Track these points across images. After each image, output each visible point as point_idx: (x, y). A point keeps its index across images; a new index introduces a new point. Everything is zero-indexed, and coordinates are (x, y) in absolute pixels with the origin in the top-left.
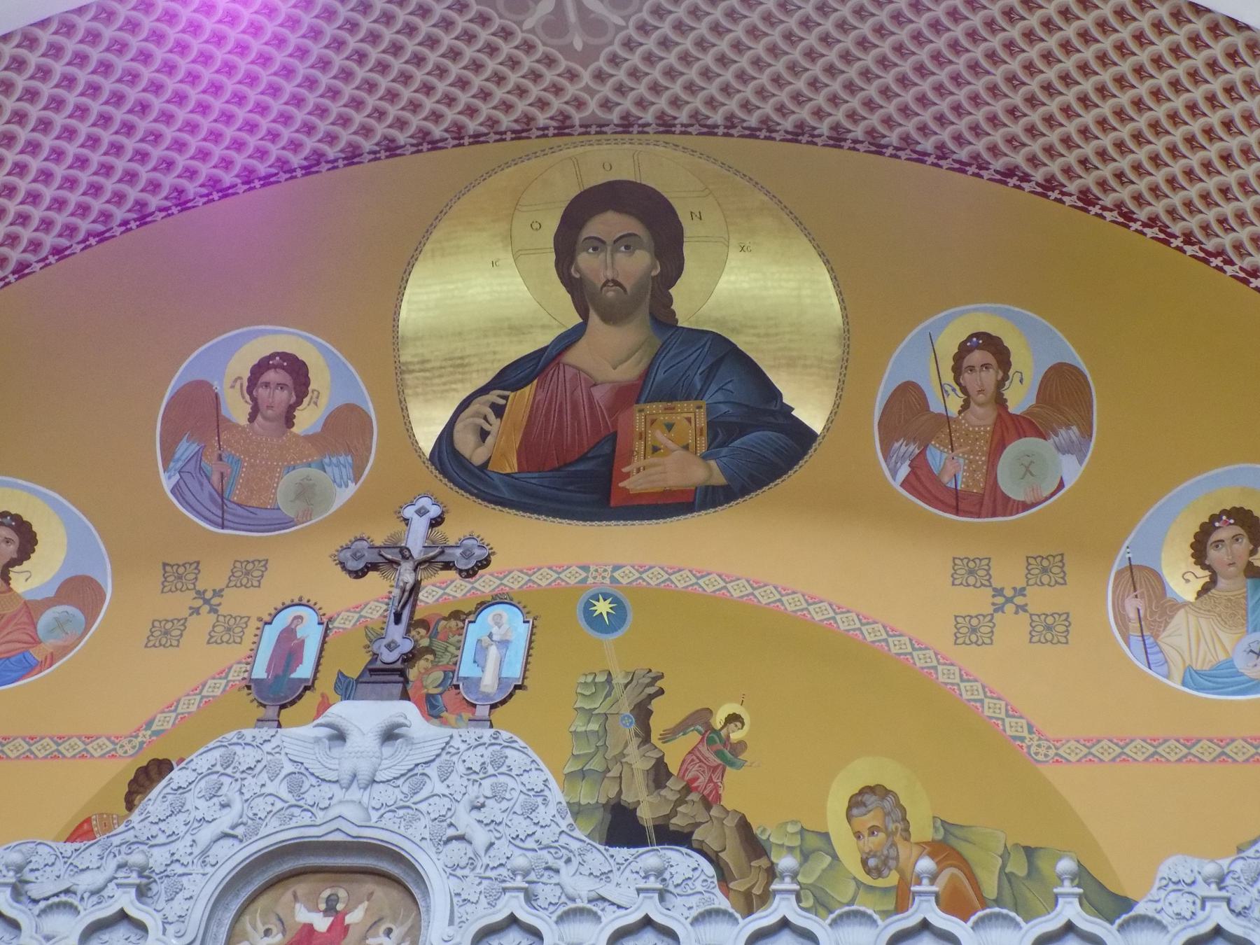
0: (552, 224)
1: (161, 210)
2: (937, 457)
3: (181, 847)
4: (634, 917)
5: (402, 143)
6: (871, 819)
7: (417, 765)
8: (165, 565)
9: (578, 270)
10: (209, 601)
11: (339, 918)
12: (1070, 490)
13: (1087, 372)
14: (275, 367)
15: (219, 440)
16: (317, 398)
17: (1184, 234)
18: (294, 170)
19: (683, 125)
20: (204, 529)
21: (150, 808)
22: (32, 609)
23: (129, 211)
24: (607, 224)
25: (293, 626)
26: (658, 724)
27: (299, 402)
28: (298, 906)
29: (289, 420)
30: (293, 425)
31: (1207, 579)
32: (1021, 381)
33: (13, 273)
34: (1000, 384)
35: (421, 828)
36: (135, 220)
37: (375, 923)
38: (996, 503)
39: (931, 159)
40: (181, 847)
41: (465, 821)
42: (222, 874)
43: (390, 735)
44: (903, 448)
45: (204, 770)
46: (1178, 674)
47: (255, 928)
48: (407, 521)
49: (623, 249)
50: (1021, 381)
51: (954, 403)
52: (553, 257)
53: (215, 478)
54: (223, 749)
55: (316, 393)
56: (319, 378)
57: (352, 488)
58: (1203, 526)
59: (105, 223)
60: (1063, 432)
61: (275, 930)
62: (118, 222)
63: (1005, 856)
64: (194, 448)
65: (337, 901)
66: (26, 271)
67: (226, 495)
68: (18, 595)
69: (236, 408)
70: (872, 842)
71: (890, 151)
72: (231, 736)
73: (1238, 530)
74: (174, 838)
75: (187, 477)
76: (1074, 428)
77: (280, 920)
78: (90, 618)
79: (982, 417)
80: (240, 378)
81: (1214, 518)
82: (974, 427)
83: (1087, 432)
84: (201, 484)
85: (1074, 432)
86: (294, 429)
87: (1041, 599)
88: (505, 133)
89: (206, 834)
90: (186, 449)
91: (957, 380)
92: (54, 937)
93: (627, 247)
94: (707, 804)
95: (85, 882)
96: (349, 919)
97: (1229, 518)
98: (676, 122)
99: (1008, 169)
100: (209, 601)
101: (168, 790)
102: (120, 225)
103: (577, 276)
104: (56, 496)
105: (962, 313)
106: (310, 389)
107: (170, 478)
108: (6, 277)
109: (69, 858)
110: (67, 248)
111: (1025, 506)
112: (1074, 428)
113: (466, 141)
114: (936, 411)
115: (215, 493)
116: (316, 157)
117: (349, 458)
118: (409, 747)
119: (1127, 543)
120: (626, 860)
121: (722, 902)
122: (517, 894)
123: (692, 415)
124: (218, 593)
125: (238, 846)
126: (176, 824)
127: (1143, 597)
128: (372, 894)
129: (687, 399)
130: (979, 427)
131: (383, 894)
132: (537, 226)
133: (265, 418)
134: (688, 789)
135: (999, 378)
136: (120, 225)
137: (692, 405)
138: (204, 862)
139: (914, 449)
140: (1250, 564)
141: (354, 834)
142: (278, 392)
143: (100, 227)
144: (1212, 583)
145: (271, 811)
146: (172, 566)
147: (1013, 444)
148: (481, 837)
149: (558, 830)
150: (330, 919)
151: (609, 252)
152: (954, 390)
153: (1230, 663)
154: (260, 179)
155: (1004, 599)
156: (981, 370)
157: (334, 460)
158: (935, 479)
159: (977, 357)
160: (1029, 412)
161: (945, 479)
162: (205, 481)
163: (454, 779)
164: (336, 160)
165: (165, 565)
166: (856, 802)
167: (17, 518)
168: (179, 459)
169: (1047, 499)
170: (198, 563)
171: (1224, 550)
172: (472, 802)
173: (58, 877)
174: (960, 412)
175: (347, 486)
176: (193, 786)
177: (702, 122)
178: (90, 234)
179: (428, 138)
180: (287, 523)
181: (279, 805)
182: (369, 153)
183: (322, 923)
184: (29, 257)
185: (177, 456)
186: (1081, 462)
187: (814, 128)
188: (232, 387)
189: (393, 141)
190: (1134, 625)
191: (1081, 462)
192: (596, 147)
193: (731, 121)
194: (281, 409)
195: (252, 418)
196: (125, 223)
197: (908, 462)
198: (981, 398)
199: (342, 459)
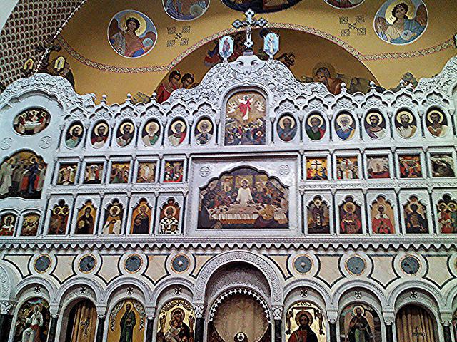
3: (213, 89)
4: (203, 103)
22: (141, 39)
35: (263, 82)
40: (213, 89)
41: (273, 80)
42: (224, 93)
43: (252, 63)
48: (247, 16)
63: (352, 80)
72: (218, 65)
87: (359, 26)
89: (218, 86)
95: (195, 97)
96: (250, 101)
111: (355, 5)
121: (329, 93)
126: (210, 84)
131: (257, 96)
148: (276, 83)
163: (268, 71)
183: (245, 102)
190: (379, 30)
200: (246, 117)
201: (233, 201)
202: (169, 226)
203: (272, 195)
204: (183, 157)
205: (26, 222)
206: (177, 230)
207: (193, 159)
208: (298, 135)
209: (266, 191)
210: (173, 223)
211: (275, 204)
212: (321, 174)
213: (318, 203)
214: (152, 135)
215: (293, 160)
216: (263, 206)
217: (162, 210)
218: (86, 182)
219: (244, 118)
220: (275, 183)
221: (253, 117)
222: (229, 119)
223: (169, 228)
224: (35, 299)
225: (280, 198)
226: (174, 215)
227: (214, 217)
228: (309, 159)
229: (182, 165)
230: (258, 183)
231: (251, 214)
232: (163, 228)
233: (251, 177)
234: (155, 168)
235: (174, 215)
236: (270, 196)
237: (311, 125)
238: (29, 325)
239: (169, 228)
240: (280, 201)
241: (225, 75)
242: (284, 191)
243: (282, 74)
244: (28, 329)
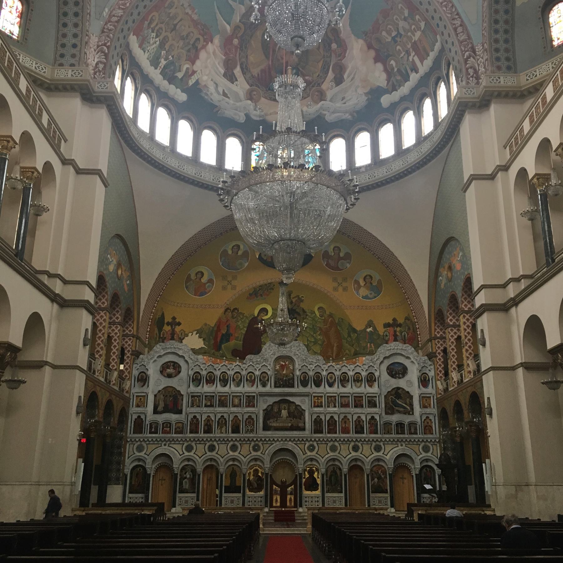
2: (330, 261)
6: (321, 311)
10: (230, 282)
11: (285, 363)
22: (205, 284)
26: (292, 297)
29: (237, 253)
38: (337, 269)
41: (297, 353)
46: (361, 296)
51: (333, 254)
57: (247, 263)
69: (230, 252)
70: (321, 313)
78: (213, 284)
83: (351, 261)
87: (344, 284)
90: (223, 258)
94: (298, 306)
100: (230, 282)
124: (231, 281)
134: (295, 304)
144: (366, 284)
148: (299, 354)
153: (367, 295)
155: (339, 284)
166: (319, 308)
205: (177, 426)
217: (246, 422)
218: (206, 406)
220: (298, 408)
224: (187, 465)
227: (271, 424)
228: (314, 397)
238: (186, 478)
242: (303, 412)
244: (186, 480)
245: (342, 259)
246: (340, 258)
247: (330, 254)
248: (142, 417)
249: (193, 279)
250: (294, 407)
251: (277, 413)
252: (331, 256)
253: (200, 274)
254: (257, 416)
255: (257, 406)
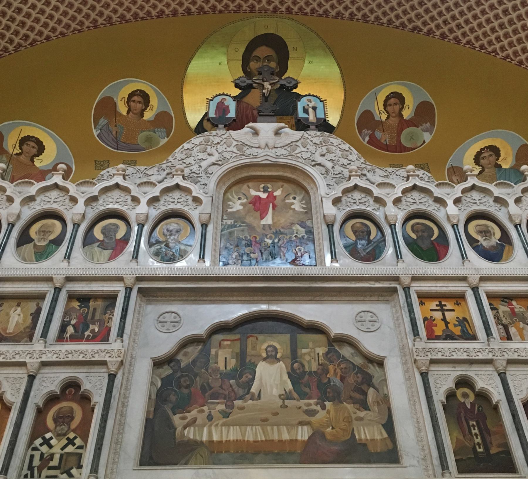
0: (242, 50)
1: (102, 24)
2: (378, 134)
5: (193, 11)
7: (292, 142)
8: (95, 161)
9: (250, 68)
12: (427, 144)
13: (433, 102)
14: (137, 95)
15: (115, 120)
16: (153, 107)
17: (224, 266)
18: (153, 16)
19: (295, 12)
20: (110, 150)
21: (176, 155)
23: (90, 23)
24: (263, 51)
25: (222, 101)
27: (146, 109)
28: (251, 190)
29: (142, 115)
30: (143, 117)
31: (481, 169)
32: (409, 108)
33: (45, 39)
34: (401, 110)
36: (92, 27)
37: (287, 195)
38: (400, 148)
39: (386, 25)
44: (366, 132)
45: (198, 143)
47: (233, 197)
49: (267, 61)
50: (409, 108)
51: (384, 117)
52: (241, 62)
53: (114, 133)
54: (204, 137)
55: (152, 106)
56: (154, 101)
57: (166, 139)
58: (477, 152)
59: (81, 26)
60: (424, 125)
61: (243, 198)
62: (86, 27)
64: (106, 121)
65: (268, 188)
66: (51, 39)
67: (118, 139)
68: (37, 167)
69: (123, 109)
71: (370, 22)
73: (491, 153)
74: (190, 165)
75: (102, 131)
76: (428, 123)
77: (244, 194)
79: (393, 121)
80: (124, 98)
81: (481, 150)
82: (391, 124)
83: (433, 124)
84: (109, 135)
85: (428, 124)
86: (144, 118)
88: (231, 11)
89: (204, 164)
90: (103, 121)
91: (385, 109)
92: (147, 193)
93: (268, 60)
97: (487, 149)
98: (293, 11)
99: (414, 28)
101: (183, 150)
102: (86, 28)
103: (249, 70)
104: (53, 133)
105: (388, 85)
106: (150, 104)
107: (96, 131)
108: (42, 40)
109: (143, 171)
110: (66, 33)
111: (412, 149)
112: (428, 123)
113: (217, 12)
114: (377, 120)
115: (114, 138)
116: (161, 12)
117: (165, 129)
118: (287, 136)
119: (450, 160)
120: (393, 171)
122: (356, 177)
123: (290, 120)
125: (220, 167)
127: (458, 175)
128: (283, 185)
129: (288, 115)
130: (393, 124)
132: (236, 50)
133: (132, 113)
135: (400, 107)
136: (86, 28)
137: (289, 117)
138: (206, 173)
139: (370, 132)
140: (496, 163)
141: (275, 161)
142: (138, 104)
143: (79, 28)
145: (231, 157)
146: (98, 162)
147: (406, 130)
148: (329, 165)
149: (361, 162)
150: (267, 194)
151: (261, 62)
152: (384, 112)
154: (140, 18)
156: (394, 105)
157: (159, 130)
158: (379, 141)
159: (392, 101)
160: (411, 119)
161: (382, 141)
162: (110, 134)
163: (308, 146)
164: (169, 15)
165: (95, 161)
167: (37, 139)
168: (100, 125)
169: (420, 147)
170: (109, 161)
171: (486, 160)
172: (320, 153)
173: (140, 177)
174: (386, 120)
175: (164, 138)
176: (194, 148)
177: (302, 12)
178: (75, 29)
179: (203, 11)
180: (143, 149)
181: (234, 155)
182: (181, 13)
183: (264, 196)
184: (51, 34)
185: (99, 124)
186: (431, 135)
187: (343, 14)
188: (121, 100)
189: (190, 10)
191: (431, 135)
192: (264, 18)
193: (313, 11)
194: (138, 111)
195: (128, 113)
196: (88, 27)
197: (368, 136)
198: (394, 115)
199: (162, 129)
200: (268, 220)
201: (241, 392)
202: (57, 457)
203: (342, 379)
204: (119, 287)
206: (80, 467)
207: (140, 290)
208: (390, 251)
209: (326, 371)
210: (70, 449)
211: (354, 401)
212: (457, 331)
213: (465, 395)
214: (43, 243)
215: (387, 301)
216: (324, 407)
217: (40, 412)
219: (263, 222)
220: (346, 352)
221: (282, 221)
222: (229, 222)
223: (55, 462)
225: (364, 387)
226: (74, 424)
227: (190, 433)
228: (423, 297)
229: (113, 305)
230: (304, 351)
231: (290, 426)
232: (36, 462)
233: (286, 337)
234: (39, 311)
235: (74, 424)
236: (337, 381)
237: (414, 236)
239: (55, 462)
240: (365, 394)
241: (221, 148)
242: (373, 370)
243: (339, 153)
245: (411, 123)
246: (404, 124)
247: (377, 118)
248: (480, 384)
249: (11, 151)
250: (321, 351)
251: (233, 374)
252: (381, 122)
253: (32, 144)
254: (112, 377)
255: (121, 334)
